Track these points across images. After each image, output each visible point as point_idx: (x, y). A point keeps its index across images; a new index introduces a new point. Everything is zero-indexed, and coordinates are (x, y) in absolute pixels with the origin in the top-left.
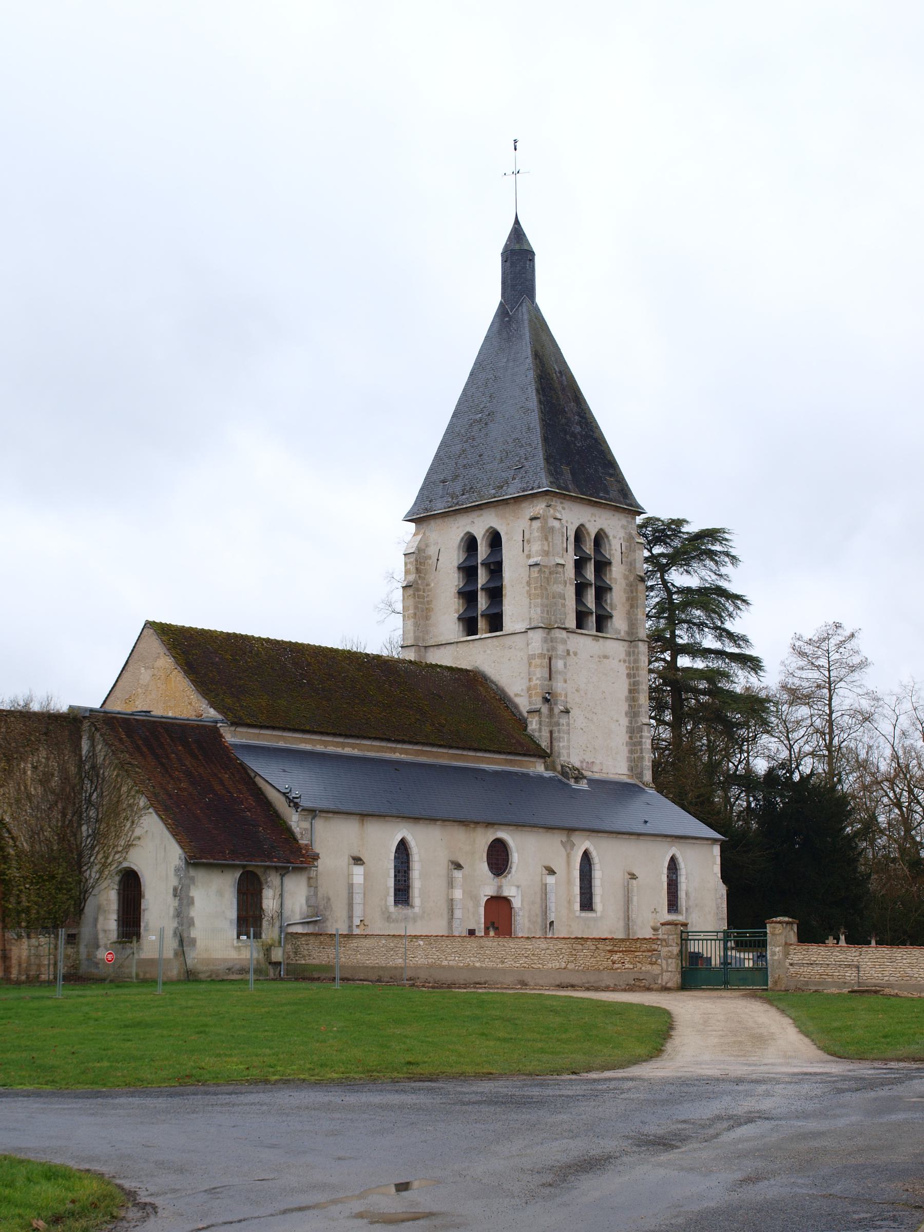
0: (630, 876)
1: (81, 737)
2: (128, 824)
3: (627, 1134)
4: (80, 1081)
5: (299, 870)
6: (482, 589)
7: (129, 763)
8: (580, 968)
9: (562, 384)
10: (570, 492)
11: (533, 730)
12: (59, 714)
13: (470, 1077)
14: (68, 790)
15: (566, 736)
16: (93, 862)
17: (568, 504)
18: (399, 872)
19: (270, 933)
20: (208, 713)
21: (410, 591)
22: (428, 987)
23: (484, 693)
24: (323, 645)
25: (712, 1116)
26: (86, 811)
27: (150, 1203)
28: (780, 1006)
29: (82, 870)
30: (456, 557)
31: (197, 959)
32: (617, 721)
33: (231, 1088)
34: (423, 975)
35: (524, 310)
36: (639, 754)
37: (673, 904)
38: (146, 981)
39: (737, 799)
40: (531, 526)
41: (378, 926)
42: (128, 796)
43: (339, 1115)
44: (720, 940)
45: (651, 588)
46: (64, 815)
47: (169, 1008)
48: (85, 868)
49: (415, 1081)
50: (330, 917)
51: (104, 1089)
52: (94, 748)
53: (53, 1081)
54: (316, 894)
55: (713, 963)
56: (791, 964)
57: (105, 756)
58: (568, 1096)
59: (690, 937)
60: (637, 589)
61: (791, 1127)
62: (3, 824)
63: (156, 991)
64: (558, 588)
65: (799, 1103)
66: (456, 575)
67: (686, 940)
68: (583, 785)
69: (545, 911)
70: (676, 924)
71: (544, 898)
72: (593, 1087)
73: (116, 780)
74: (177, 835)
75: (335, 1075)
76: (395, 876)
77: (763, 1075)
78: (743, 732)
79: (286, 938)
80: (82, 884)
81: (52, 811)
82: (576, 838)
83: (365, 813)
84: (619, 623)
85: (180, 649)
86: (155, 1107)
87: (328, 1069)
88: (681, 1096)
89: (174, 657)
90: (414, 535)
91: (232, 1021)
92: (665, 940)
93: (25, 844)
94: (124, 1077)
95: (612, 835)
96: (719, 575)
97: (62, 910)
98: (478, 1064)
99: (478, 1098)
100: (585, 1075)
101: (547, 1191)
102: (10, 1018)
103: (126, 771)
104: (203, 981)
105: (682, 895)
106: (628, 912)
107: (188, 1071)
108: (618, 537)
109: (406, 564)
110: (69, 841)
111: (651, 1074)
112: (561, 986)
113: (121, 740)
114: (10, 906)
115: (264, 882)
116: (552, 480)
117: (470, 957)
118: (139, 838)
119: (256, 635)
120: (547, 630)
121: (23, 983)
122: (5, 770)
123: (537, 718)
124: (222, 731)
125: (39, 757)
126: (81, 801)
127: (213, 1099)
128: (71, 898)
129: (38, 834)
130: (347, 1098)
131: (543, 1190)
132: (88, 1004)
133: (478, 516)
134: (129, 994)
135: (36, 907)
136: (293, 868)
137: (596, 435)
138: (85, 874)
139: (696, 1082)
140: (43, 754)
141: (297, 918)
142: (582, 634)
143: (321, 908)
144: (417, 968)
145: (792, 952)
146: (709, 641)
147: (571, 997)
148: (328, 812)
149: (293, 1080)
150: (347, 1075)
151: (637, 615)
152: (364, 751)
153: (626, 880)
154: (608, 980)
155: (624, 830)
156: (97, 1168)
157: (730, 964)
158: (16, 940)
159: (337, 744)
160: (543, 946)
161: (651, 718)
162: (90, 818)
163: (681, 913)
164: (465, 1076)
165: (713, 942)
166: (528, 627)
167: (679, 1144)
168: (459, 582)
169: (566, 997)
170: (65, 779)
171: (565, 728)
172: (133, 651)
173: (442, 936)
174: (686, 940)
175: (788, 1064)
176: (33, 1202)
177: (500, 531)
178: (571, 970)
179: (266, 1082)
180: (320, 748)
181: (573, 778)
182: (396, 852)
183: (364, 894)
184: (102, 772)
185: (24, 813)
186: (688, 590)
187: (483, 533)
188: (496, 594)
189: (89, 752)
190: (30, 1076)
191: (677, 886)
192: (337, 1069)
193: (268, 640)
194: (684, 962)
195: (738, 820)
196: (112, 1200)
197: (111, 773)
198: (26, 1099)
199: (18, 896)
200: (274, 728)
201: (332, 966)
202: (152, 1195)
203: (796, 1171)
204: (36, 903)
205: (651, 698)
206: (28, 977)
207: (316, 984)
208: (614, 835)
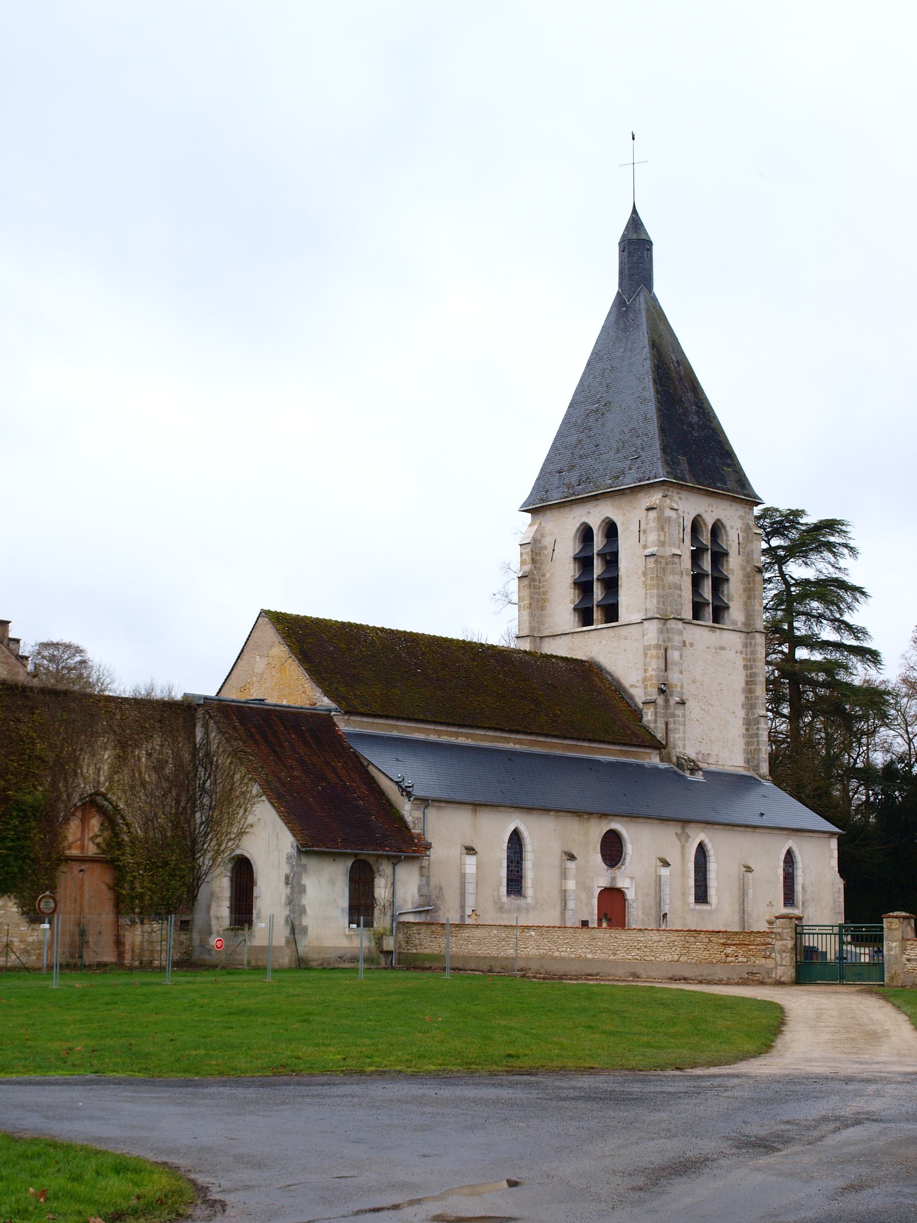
0: (745, 869)
1: (195, 725)
2: (241, 812)
3: (727, 1134)
4: (174, 1069)
5: (411, 859)
6: (598, 580)
7: (243, 751)
8: (693, 961)
9: (679, 374)
10: (687, 482)
11: (649, 721)
12: (174, 701)
13: (570, 1071)
14: (181, 777)
15: (681, 727)
16: (206, 849)
17: (684, 494)
18: (512, 862)
19: (381, 922)
20: (322, 701)
21: (526, 582)
22: (539, 978)
23: (599, 684)
24: (438, 635)
25: (817, 1117)
27: (220, 1201)
28: (895, 1002)
29: (196, 856)
30: (571, 548)
31: (309, 947)
32: (734, 713)
33: (325, 1079)
34: (534, 966)
35: (642, 299)
36: (755, 746)
37: (789, 898)
38: (257, 969)
39: (856, 793)
40: (647, 516)
41: (490, 917)
42: (241, 784)
43: (430, 1110)
44: (835, 934)
45: (769, 580)
46: (178, 802)
47: (275, 995)
48: (199, 855)
49: (514, 1075)
50: (442, 907)
51: (196, 1078)
53: (146, 1069)
54: (428, 883)
55: (828, 957)
56: (908, 960)
57: (219, 744)
58: (669, 1093)
59: (805, 931)
60: (754, 581)
61: (900, 1130)
62: (118, 810)
63: (266, 979)
64: (671, 579)
65: (910, 1105)
66: (572, 566)
67: (801, 934)
68: (699, 777)
69: (659, 903)
70: (791, 918)
71: (658, 890)
72: (696, 1084)
73: (230, 767)
74: (289, 823)
75: (432, 1067)
76: (508, 866)
77: (874, 1074)
78: (863, 725)
79: (397, 927)
80: (196, 871)
81: (166, 798)
82: (691, 830)
83: (478, 802)
84: (736, 614)
85: (295, 638)
86: (245, 1098)
87: (425, 1061)
88: (787, 1095)
89: (288, 646)
90: (530, 525)
91: (337, 1009)
92: (779, 934)
93: (139, 831)
94: (219, 1065)
95: (727, 828)
96: (837, 568)
97: (176, 897)
98: (580, 1058)
99: (577, 1094)
100: (689, 1071)
101: (636, 1195)
102: (116, 1003)
103: (240, 758)
104: (315, 969)
105: (798, 888)
106: (743, 905)
107: (284, 1060)
108: (735, 528)
109: (521, 554)
110: (183, 828)
111: (757, 1071)
112: (673, 979)
113: (234, 728)
114: (124, 892)
116: (668, 470)
117: (581, 948)
118: (252, 826)
119: (371, 625)
120: (663, 621)
121: (136, 968)
122: (120, 756)
123: (652, 709)
124: (335, 720)
125: (153, 744)
126: (195, 789)
127: (304, 1090)
128: (185, 884)
129: (152, 821)
130: (442, 1091)
131: (632, 1195)
132: (195, 991)
133: (594, 507)
134: (238, 981)
135: (150, 893)
136: (405, 857)
137: (713, 425)
138: (198, 862)
139: (804, 1081)
140: (157, 740)
141: (409, 907)
142: (698, 625)
143: (434, 897)
144: (528, 958)
145: (909, 947)
146: (827, 633)
147: (682, 990)
148: (440, 801)
149: (389, 1072)
150: (445, 1067)
151: (754, 606)
152: (478, 740)
153: (741, 873)
154: (721, 973)
155: (740, 822)
156: (174, 1161)
157: (846, 959)
158: (130, 926)
159: (451, 734)
160: (656, 938)
161: (768, 710)
162: (204, 805)
163: (797, 907)
164: (565, 1071)
165: (829, 936)
166: (644, 618)
167: (780, 1146)
168: (575, 572)
169: (677, 989)
170: (179, 766)
171: (680, 719)
172: (248, 639)
173: (554, 927)
174: (801, 934)
175: (900, 1063)
176: (97, 1197)
177: (616, 522)
178: (683, 963)
179: (362, 1073)
180: (433, 738)
181: (688, 769)
182: (509, 842)
183: (477, 884)
184: (215, 759)
185: (138, 800)
186: (806, 582)
187: (599, 523)
188: (612, 584)
189: (203, 740)
190: (124, 1063)
191: (793, 880)
192: (434, 1060)
193: (383, 630)
194: (798, 957)
195: (856, 814)
196: (180, 1197)
197: (223, 761)
198: (116, 1087)
199: (132, 882)
200: (387, 717)
201: (443, 956)
202: (224, 1191)
203: (903, 1178)
204: (150, 889)
205: (768, 690)
206: (141, 962)
207: (427, 974)
208: (730, 828)
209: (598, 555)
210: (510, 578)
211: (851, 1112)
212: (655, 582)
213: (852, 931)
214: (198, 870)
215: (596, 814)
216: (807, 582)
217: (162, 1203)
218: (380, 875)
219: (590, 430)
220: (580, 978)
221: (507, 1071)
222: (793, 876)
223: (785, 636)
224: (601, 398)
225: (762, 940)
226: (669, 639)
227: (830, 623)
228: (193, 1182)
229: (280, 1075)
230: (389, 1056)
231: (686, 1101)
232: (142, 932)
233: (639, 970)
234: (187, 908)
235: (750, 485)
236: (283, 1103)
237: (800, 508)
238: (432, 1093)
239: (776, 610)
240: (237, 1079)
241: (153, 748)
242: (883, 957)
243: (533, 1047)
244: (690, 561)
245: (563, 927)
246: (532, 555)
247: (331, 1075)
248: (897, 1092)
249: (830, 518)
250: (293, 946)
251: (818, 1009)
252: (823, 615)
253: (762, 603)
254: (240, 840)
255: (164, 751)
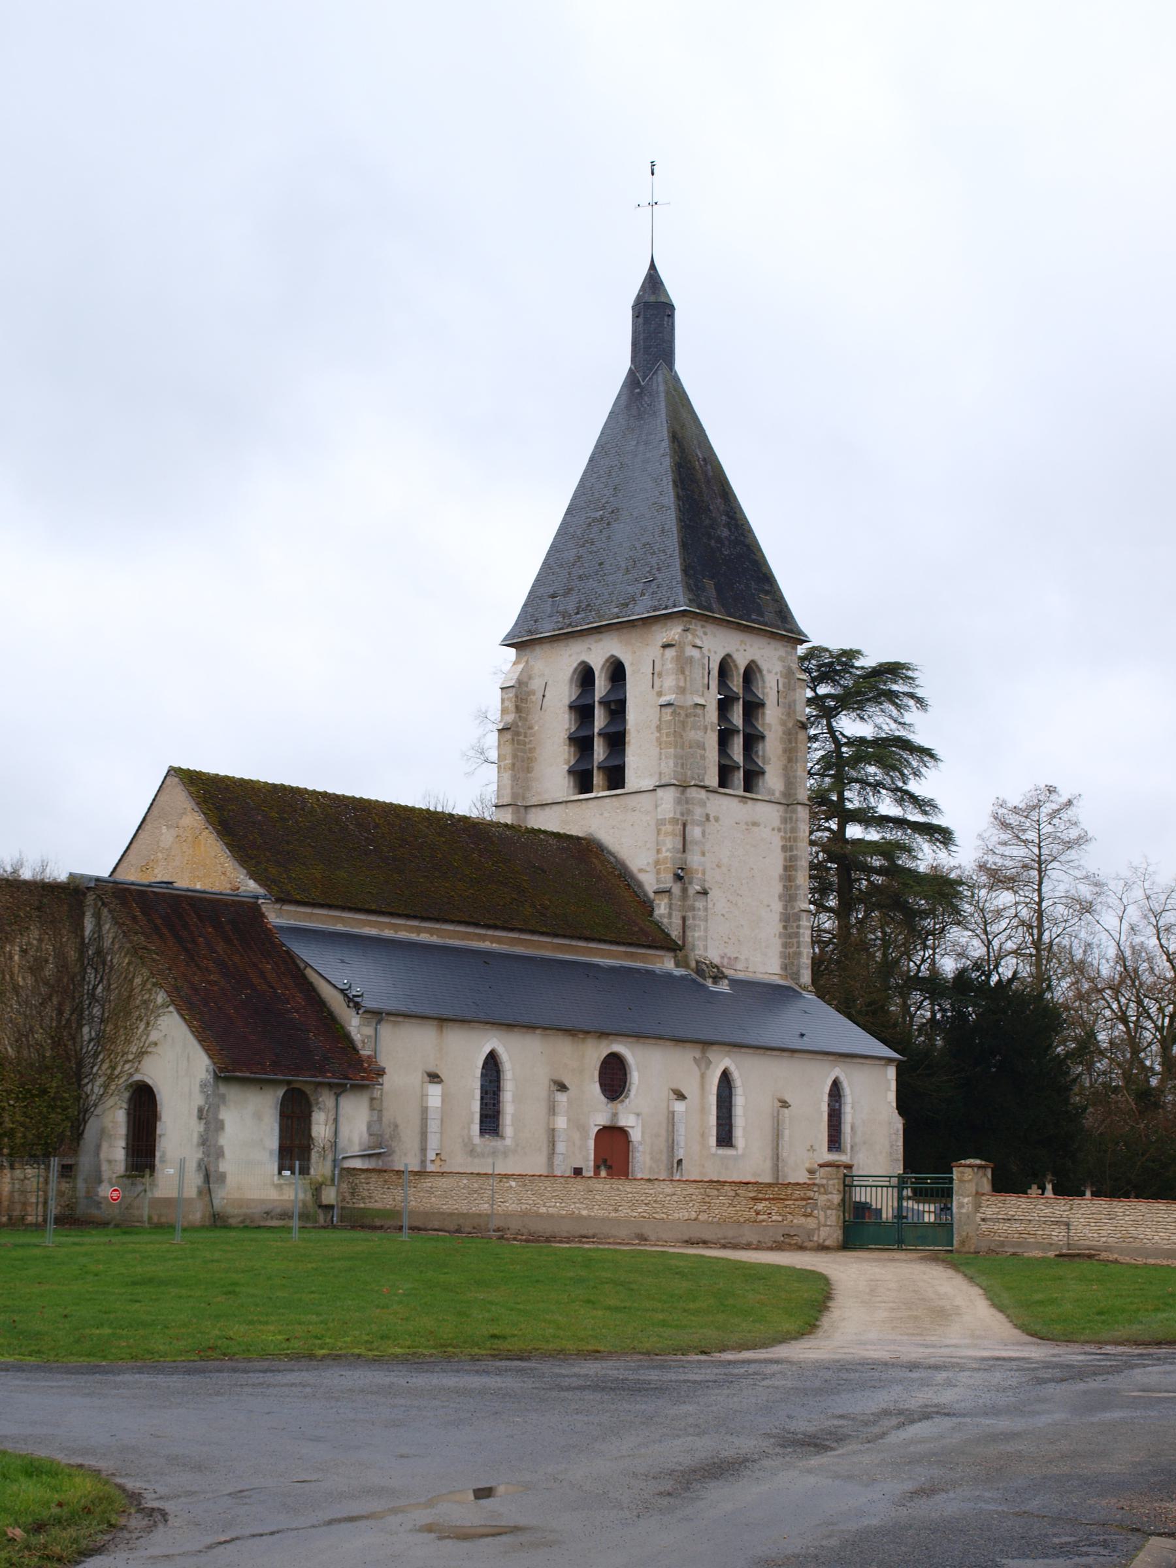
1: (83, 914)
2: (142, 1026)
3: (769, 1431)
4: (74, 1351)
5: (359, 1088)
6: (599, 734)
9: (706, 475)
11: (661, 916)
13: (571, 1355)
14: (65, 980)
15: (702, 924)
16: (96, 1074)
17: (711, 628)
18: (486, 1094)
19: (320, 1168)
21: (508, 736)
22: (521, 1240)
26: (88, 1008)
27: (159, 1509)
28: (967, 1272)
30: (567, 693)
31: (227, 1199)
32: (768, 906)
33: (266, 1364)
34: (515, 1225)
35: (660, 379)
36: (794, 949)
37: (835, 1141)
38: (161, 1227)
39: (919, 1008)
40: (663, 655)
41: (458, 1162)
42: (142, 990)
44: (893, 1187)
45: (815, 738)
46: (60, 1013)
48: (86, 1080)
49: (501, 1360)
50: (397, 1149)
52: (100, 928)
53: (39, 1352)
54: (380, 1119)
55: (884, 1216)
56: (983, 1220)
57: (114, 938)
58: (695, 1382)
59: (855, 1183)
60: (796, 739)
61: (977, 1426)
64: (693, 735)
66: (567, 716)
67: (851, 1186)
68: (724, 987)
69: (671, 1146)
70: (838, 1166)
71: (670, 1129)
72: (727, 1371)
75: (399, 1350)
76: (482, 1098)
78: (928, 923)
79: (340, 1174)
80: (82, 1101)
81: (45, 1008)
83: (445, 1017)
84: (772, 780)
85: (212, 804)
86: (169, 1387)
88: (839, 1385)
89: (205, 814)
91: (269, 1278)
92: (823, 1186)
93: (9, 1049)
94: (130, 1347)
95: (759, 1051)
96: (900, 723)
98: (582, 1340)
99: (581, 1382)
101: (665, 1501)
104: (234, 1228)
105: (846, 1128)
106: (777, 1149)
107: (212, 1341)
108: (774, 672)
109: (503, 700)
110: (66, 1046)
111: (801, 1356)
112: (689, 1242)
113: (134, 918)
115: (313, 1102)
118: (156, 1044)
119: (310, 788)
123: (666, 901)
124: (264, 910)
125: (29, 938)
126: (83, 996)
128: (67, 1118)
129: (27, 1036)
130: (414, 1380)
132: (86, 1254)
133: (596, 642)
134: (139, 1243)
135: (22, 1129)
137: (748, 541)
138: (85, 1089)
139: (859, 1367)
140: (35, 933)
141: (355, 1150)
143: (387, 1136)
144: (507, 1215)
145: (984, 1203)
146: (887, 806)
149: (345, 1356)
150: (415, 1350)
151: (796, 771)
154: (750, 1235)
156: (91, 1463)
157: (906, 1217)
159: (411, 929)
160: (669, 1190)
162: (93, 1017)
164: (565, 1355)
165: (885, 1189)
166: (657, 784)
167: (834, 1445)
168: (570, 724)
170: (62, 967)
171: (701, 913)
172: (152, 804)
173: (540, 1176)
174: (851, 1186)
177: (624, 661)
178: (703, 1222)
179: (311, 1357)
180: (388, 933)
181: (710, 977)
182: (483, 1068)
184: (109, 958)
185: (9, 1009)
188: (617, 741)
190: (9, 1345)
191: (840, 1118)
192: (401, 1342)
193: (325, 795)
195: (919, 1036)
196: (110, 1504)
197: (120, 960)
200: (330, 907)
201: (398, 1212)
202: (161, 1498)
204: (22, 1124)
206: (10, 1219)
208: (762, 1051)
209: (600, 703)
210: (487, 730)
211: (918, 1404)
212: (671, 739)
213: (912, 1183)
214: (85, 1101)
215: (595, 1032)
216: (862, 740)
217: (89, 1512)
218: (320, 1108)
219: (592, 543)
220: (572, 1241)
221: (492, 1355)
222: (840, 1113)
223: (833, 809)
224: (607, 503)
225: (802, 1193)
226: (689, 812)
227: (890, 794)
228: (121, 1488)
229: (208, 1359)
230: (344, 1337)
231: (717, 1391)
232: (12, 1179)
233: (647, 1231)
234: (70, 1148)
235: (793, 617)
236: (218, 1394)
237: (855, 648)
238: (402, 1382)
239: (823, 775)
240: (155, 1364)
241: (29, 943)
242: (951, 1216)
243: (523, 1326)
244: (717, 713)
245: (550, 1176)
246: (516, 702)
247: (273, 1360)
248: (971, 1381)
249: (893, 661)
250: (207, 1199)
251: (872, 1280)
252: (882, 784)
253: (806, 767)
254: (140, 1062)
255: (43, 946)
